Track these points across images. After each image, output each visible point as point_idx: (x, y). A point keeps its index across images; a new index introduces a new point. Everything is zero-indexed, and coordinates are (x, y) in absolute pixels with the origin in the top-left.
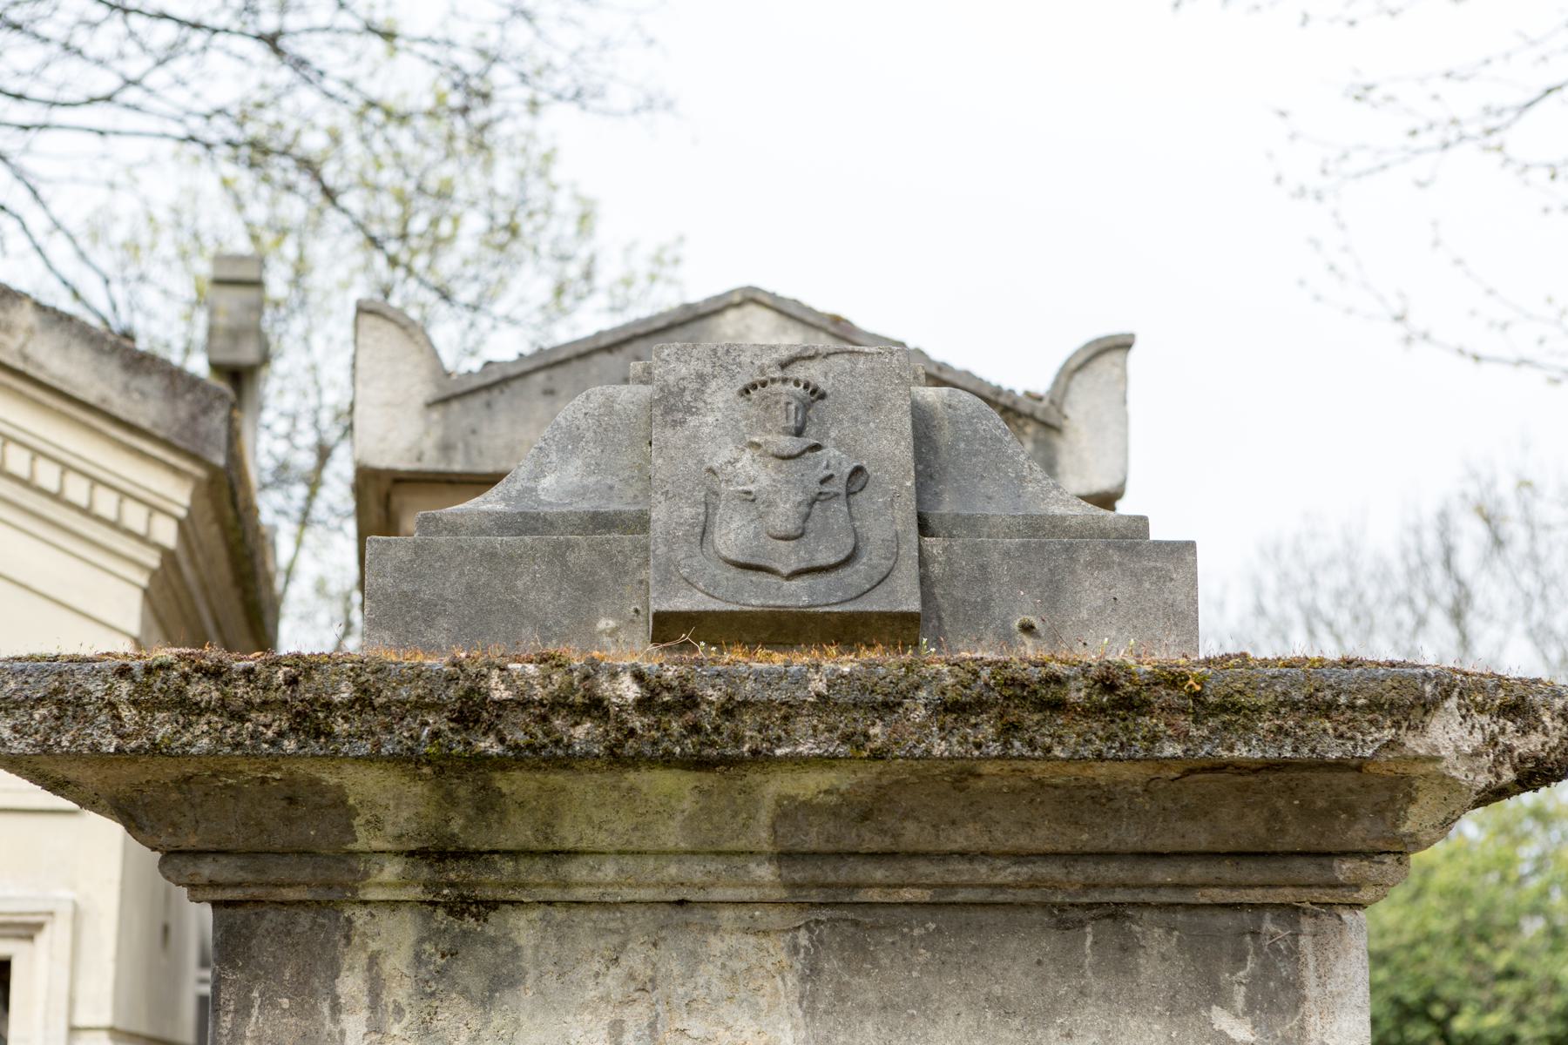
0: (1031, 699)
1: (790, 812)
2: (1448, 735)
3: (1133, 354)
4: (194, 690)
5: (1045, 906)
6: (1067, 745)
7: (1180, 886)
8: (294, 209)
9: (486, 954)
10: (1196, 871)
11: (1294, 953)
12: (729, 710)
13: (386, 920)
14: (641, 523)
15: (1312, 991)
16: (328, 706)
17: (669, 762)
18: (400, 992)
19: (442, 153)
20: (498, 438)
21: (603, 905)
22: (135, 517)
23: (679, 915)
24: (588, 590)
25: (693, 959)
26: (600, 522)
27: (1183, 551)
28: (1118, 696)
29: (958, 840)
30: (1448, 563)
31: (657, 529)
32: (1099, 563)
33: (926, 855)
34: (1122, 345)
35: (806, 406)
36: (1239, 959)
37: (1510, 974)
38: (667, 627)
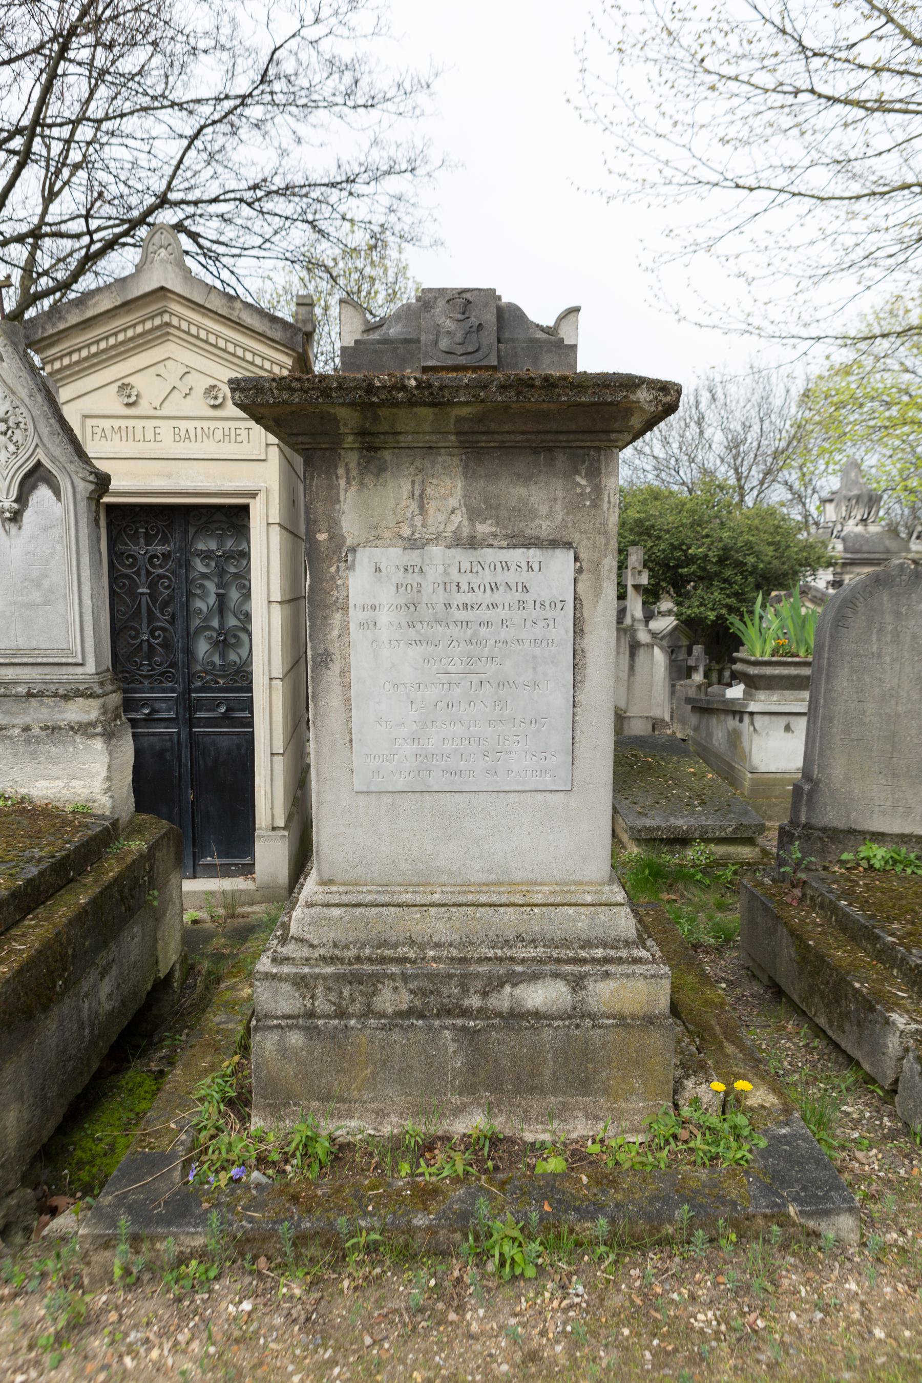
0: (525, 384)
1: (460, 420)
2: (643, 395)
4: (293, 385)
5: (530, 447)
6: (535, 396)
7: (567, 441)
8: (324, 285)
9: (377, 462)
10: (572, 437)
11: (599, 460)
12: (441, 388)
13: (350, 453)
14: (418, 341)
15: (603, 471)
16: (331, 389)
17: (424, 404)
18: (354, 473)
21: (409, 448)
23: (429, 451)
25: (434, 463)
26: (406, 341)
27: (574, 348)
28: (549, 383)
29: (506, 428)
30: (697, 407)
31: (423, 342)
32: (549, 351)
33: (497, 433)
34: (577, 310)
35: (465, 306)
36: (584, 462)
37: (707, 536)
38: (425, 370)
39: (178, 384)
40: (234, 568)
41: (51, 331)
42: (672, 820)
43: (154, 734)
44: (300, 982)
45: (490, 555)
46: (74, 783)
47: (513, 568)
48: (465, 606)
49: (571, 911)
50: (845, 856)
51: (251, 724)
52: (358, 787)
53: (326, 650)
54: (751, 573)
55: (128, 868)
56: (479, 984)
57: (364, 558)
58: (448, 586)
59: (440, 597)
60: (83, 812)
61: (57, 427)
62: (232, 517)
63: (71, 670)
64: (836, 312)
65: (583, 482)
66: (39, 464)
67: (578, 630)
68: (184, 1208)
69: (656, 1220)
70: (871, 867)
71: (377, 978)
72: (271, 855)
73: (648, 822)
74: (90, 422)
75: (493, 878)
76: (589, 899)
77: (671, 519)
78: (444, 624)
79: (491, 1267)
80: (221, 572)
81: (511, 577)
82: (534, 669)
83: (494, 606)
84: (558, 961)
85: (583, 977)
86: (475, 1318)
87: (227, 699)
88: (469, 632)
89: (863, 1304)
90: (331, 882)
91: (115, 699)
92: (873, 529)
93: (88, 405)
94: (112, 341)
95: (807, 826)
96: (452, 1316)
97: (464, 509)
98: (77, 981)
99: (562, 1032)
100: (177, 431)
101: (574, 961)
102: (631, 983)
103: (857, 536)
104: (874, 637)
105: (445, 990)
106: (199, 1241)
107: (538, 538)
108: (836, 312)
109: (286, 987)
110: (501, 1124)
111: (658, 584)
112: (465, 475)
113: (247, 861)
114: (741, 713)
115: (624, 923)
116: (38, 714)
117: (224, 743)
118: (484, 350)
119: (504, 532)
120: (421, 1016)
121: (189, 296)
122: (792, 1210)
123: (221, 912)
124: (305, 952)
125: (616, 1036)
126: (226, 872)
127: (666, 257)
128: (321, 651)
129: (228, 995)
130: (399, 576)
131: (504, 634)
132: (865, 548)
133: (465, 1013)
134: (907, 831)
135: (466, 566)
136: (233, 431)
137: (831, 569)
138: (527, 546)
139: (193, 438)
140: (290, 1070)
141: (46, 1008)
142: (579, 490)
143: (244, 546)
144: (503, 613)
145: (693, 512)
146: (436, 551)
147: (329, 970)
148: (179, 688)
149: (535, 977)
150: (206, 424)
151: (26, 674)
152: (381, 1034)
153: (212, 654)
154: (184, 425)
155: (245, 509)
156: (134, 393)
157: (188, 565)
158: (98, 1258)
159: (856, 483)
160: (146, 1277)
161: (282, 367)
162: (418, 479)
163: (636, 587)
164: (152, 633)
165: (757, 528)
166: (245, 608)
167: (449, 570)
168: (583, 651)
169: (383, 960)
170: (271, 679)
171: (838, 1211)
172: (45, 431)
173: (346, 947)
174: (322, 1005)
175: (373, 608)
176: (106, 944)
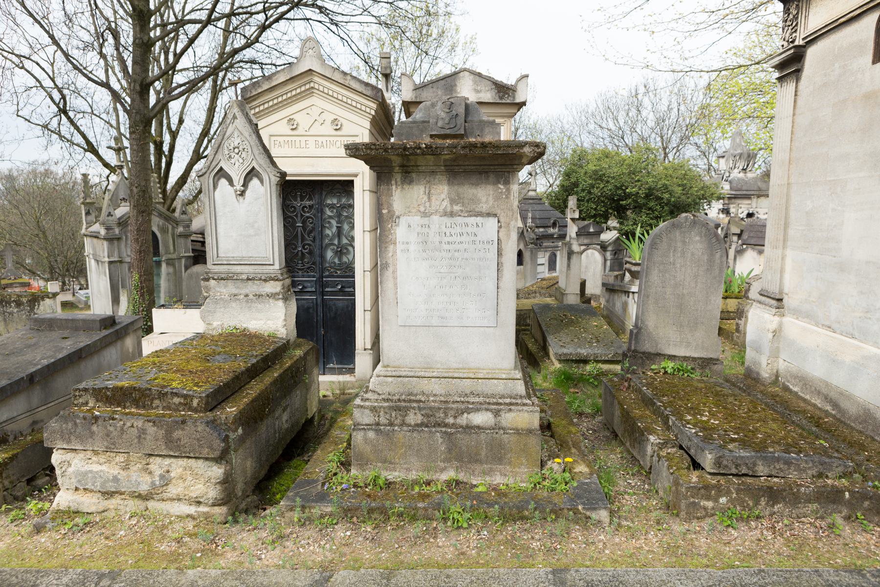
1: (445, 160)
2: (527, 150)
12: (436, 148)
18: (399, 183)
19: (217, 453)
20: (426, 95)
22: (368, 110)
24: (422, 131)
25: (434, 179)
26: (424, 122)
28: (484, 145)
34: (527, 76)
37: (639, 181)
38: (432, 136)
40: (345, 213)
41: (254, 93)
42: (579, 350)
43: (304, 299)
44: (374, 409)
45: (459, 220)
46: (269, 322)
48: (449, 243)
49: (496, 381)
50: (653, 367)
54: (666, 204)
55: (295, 362)
56: (452, 413)
57: (403, 221)
59: (437, 239)
60: (272, 336)
61: (262, 150)
62: (345, 187)
63: (268, 267)
64: (702, 53)
65: (502, 187)
66: (253, 168)
67: (500, 254)
68: (322, 497)
69: (520, 509)
70: (666, 372)
71: (407, 409)
72: (362, 361)
73: (565, 351)
74: (273, 138)
75: (461, 366)
76: (504, 376)
77: (615, 170)
79: (449, 524)
80: (339, 215)
81: (470, 230)
84: (489, 403)
85: (499, 411)
86: (441, 541)
87: (342, 281)
89: (604, 543)
91: (288, 281)
92: (750, 175)
93: (272, 130)
94: (285, 97)
95: (635, 351)
96: (432, 540)
98: (274, 411)
99: (490, 435)
101: (496, 405)
102: (521, 414)
103: (739, 179)
104: (671, 254)
105: (437, 415)
106: (329, 509)
108: (702, 53)
109: (367, 411)
110: (461, 477)
111: (607, 211)
112: (449, 184)
113: (351, 366)
114: (629, 292)
115: (520, 388)
116: (253, 288)
117: (340, 304)
118: (458, 126)
120: (427, 426)
122: (580, 507)
123: (338, 392)
124: (376, 397)
125: (514, 438)
126: (340, 372)
127: (596, 25)
129: (341, 424)
130: (419, 229)
131: (466, 255)
132: (744, 188)
133: (446, 425)
134: (687, 355)
135: (449, 225)
137: (721, 201)
138: (476, 216)
140: (368, 449)
141: (262, 420)
143: (351, 201)
145: (630, 165)
146: (435, 218)
147: (386, 404)
148: (317, 275)
149: (478, 410)
150: (332, 139)
151: (250, 269)
152: (408, 434)
153: (334, 258)
154: (320, 139)
155: (351, 183)
156: (295, 123)
157: (322, 212)
158: (288, 514)
159: (740, 145)
160: (307, 523)
162: (428, 186)
163: (573, 220)
164: (303, 247)
165: (671, 176)
166: (351, 234)
169: (410, 401)
171: (600, 508)
172: (256, 152)
173: (394, 395)
174: (383, 420)
175: (407, 243)
176: (285, 396)
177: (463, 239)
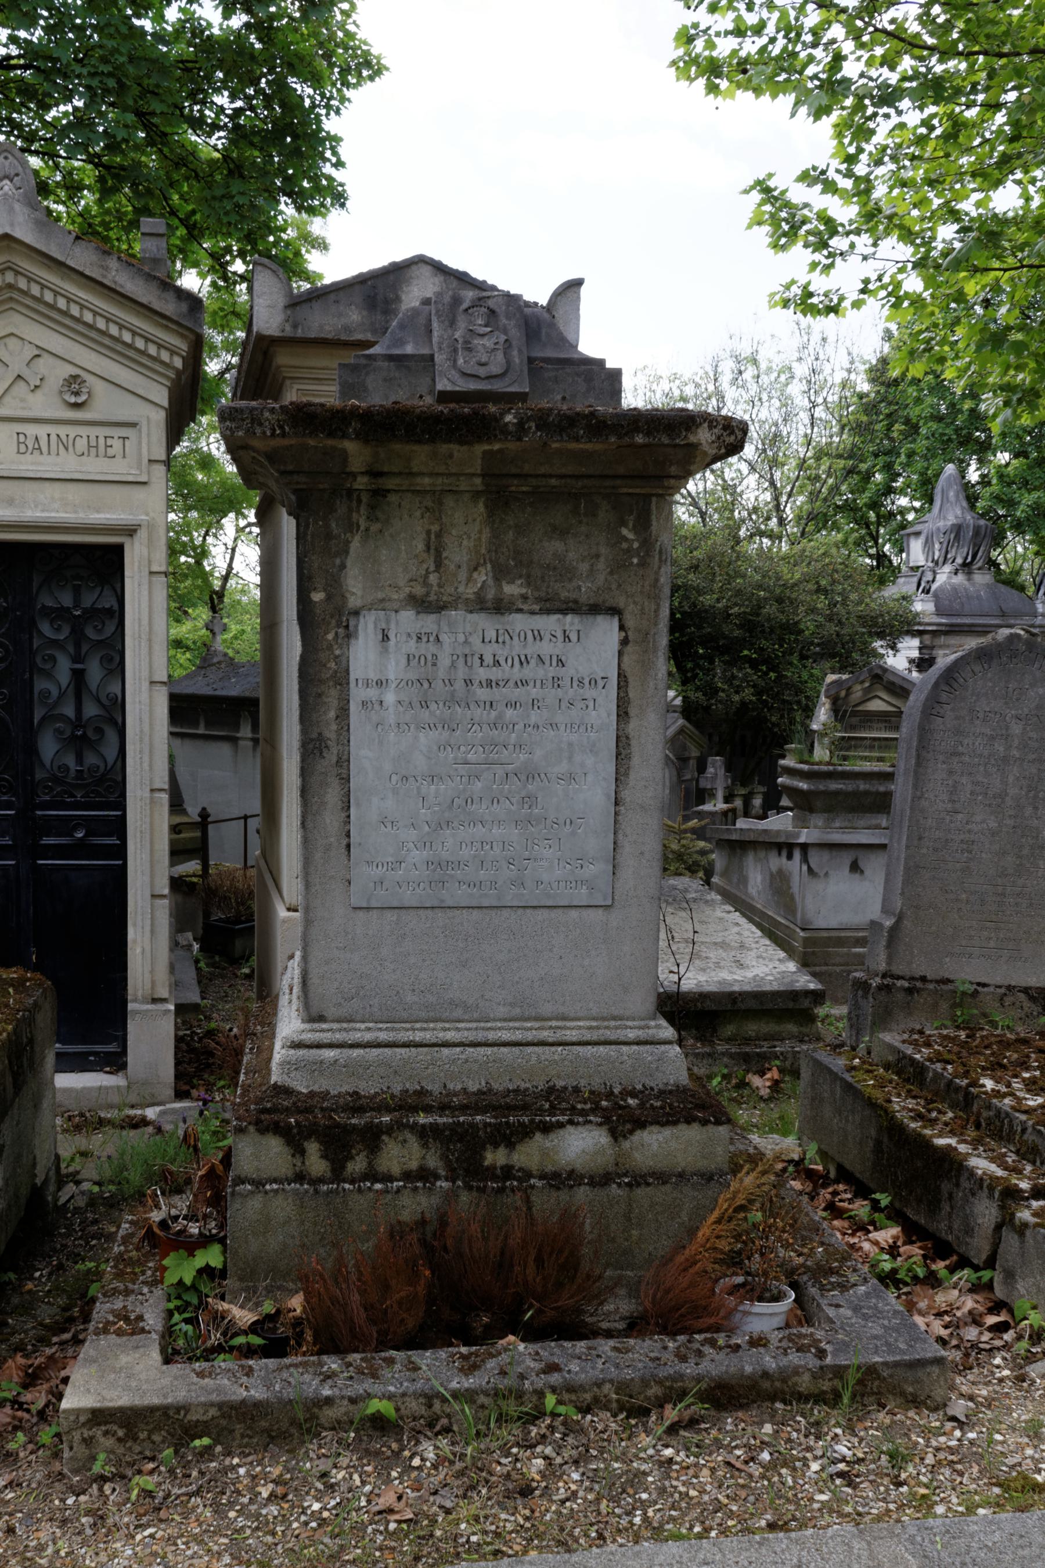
3: (583, 290)
10: (618, 482)
22: (165, 356)
34: (578, 283)
39: (26, 373)
45: (519, 622)
47: (547, 637)
48: (489, 683)
51: (121, 852)
52: (355, 901)
53: (320, 734)
57: (367, 627)
58: (469, 659)
65: (631, 536)
75: (517, 1011)
76: (632, 1035)
78: (463, 704)
80: (78, 635)
81: (546, 648)
82: (570, 758)
83: (524, 683)
88: (493, 714)
90: (321, 1019)
97: (489, 566)
100: (22, 438)
103: (955, 589)
107: (576, 602)
113: (112, 1048)
119: (536, 594)
121: (44, 249)
128: (314, 735)
130: (412, 646)
135: (491, 634)
136: (101, 441)
138: (564, 612)
139: (45, 449)
142: (625, 545)
144: (535, 692)
150: (63, 431)
154: (31, 430)
155: (118, 551)
161: (173, 353)
167: (470, 639)
168: (627, 738)
170: (152, 790)
177: (529, 672)
